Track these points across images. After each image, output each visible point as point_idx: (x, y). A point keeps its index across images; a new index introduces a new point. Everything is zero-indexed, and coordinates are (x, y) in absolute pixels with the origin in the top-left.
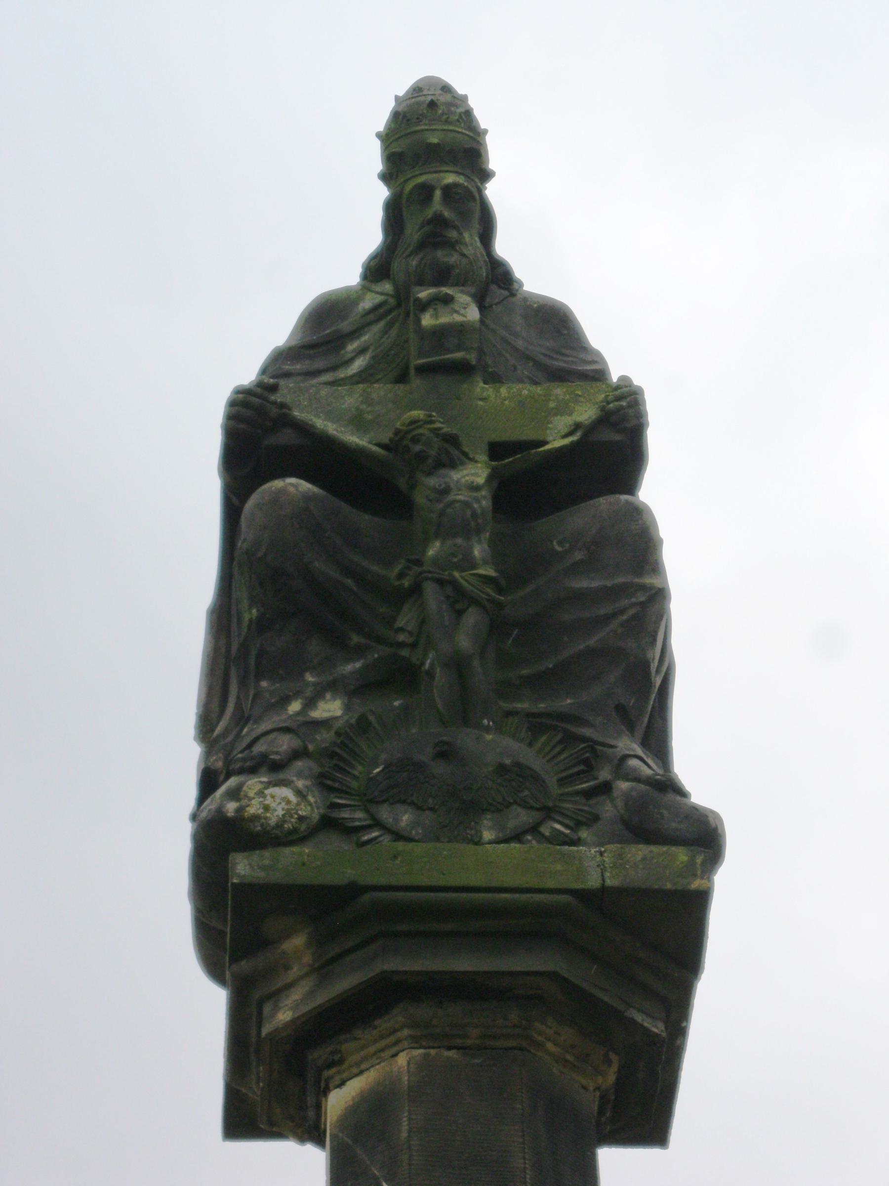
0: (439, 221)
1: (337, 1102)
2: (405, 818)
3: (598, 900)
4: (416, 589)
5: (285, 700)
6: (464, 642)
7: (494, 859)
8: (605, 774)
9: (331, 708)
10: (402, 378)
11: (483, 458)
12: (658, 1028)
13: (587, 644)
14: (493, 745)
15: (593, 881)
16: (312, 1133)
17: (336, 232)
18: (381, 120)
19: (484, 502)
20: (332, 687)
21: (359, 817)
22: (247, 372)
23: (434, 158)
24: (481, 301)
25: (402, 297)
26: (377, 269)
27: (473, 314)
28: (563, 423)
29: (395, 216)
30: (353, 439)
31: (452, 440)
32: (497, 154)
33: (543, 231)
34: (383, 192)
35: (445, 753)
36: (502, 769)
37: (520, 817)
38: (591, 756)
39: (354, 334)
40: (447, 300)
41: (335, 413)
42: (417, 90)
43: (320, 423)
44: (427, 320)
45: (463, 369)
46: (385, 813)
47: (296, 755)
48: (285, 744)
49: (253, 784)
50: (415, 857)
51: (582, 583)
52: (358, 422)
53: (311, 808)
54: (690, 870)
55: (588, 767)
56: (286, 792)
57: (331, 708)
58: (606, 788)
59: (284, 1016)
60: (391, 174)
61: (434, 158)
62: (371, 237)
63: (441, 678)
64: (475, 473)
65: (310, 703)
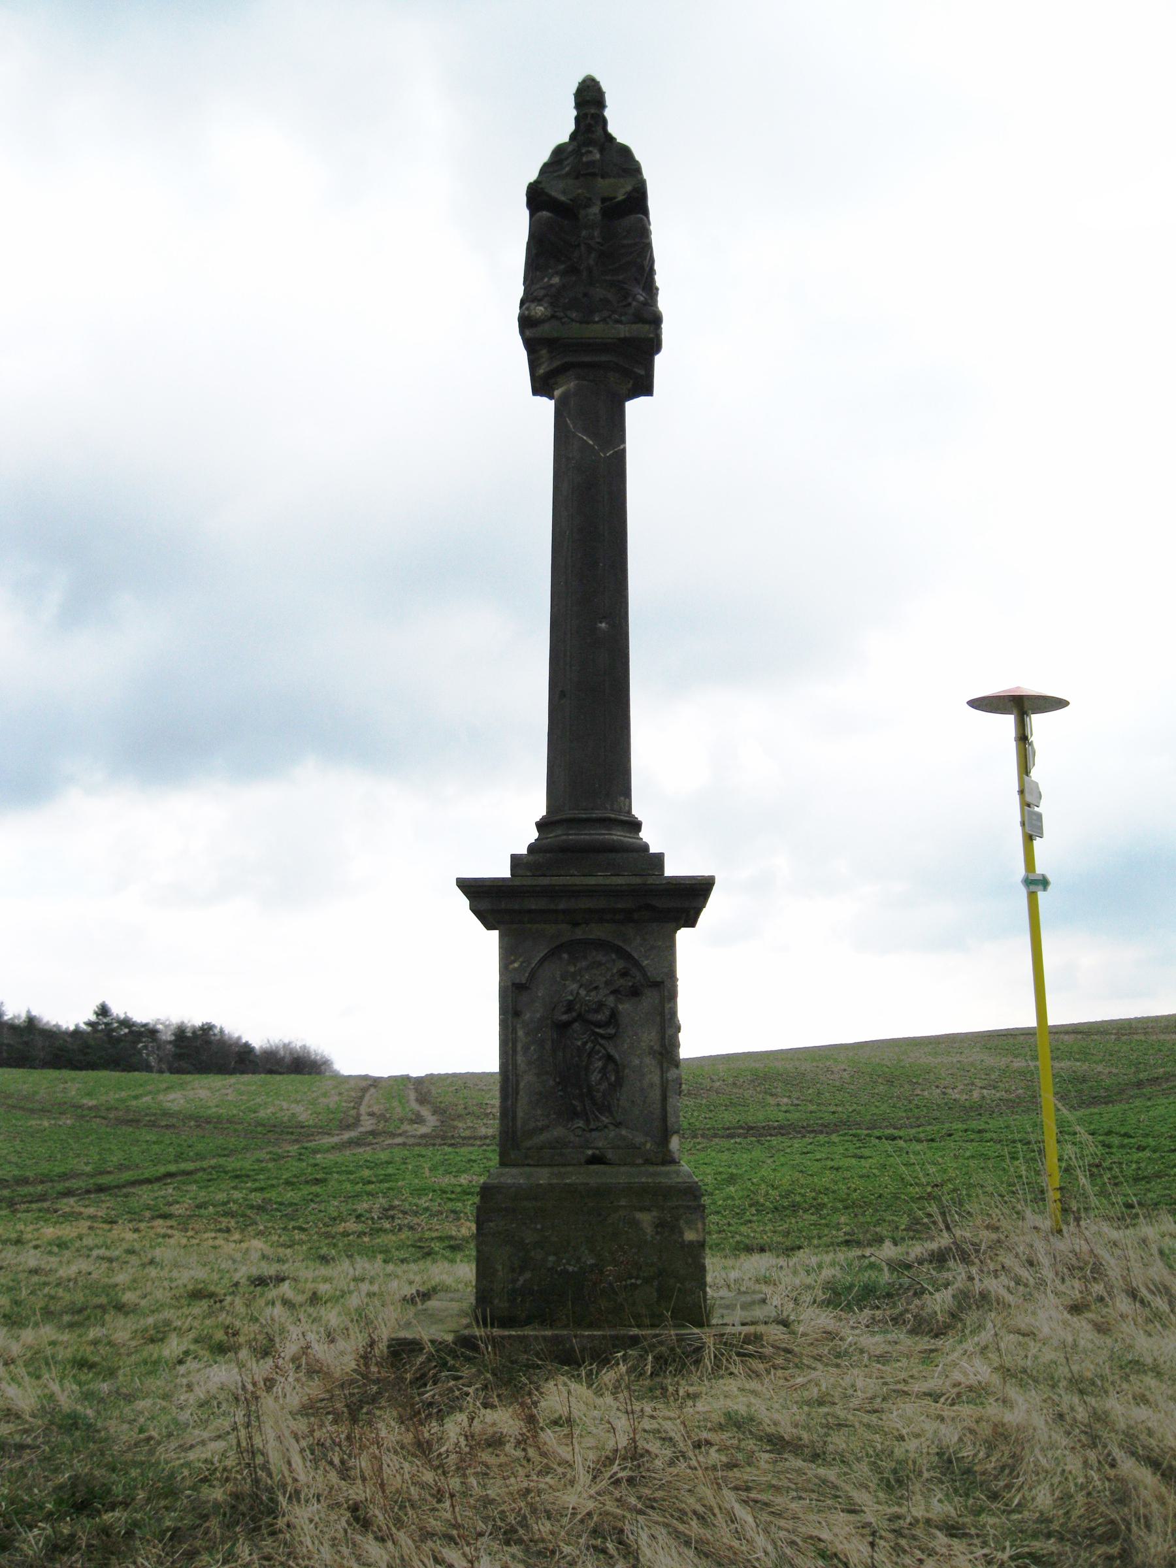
0: (590, 125)
1: (557, 393)
2: (574, 315)
3: (624, 341)
4: (579, 245)
5: (543, 279)
6: (591, 262)
7: (598, 330)
8: (630, 300)
9: (556, 280)
10: (577, 178)
11: (599, 203)
12: (642, 372)
13: (67, 1185)
14: (599, 293)
15: (622, 336)
16: (551, 397)
17: (561, 125)
18: (574, 90)
19: (599, 217)
20: (557, 273)
21: (562, 314)
22: (533, 175)
23: (590, 98)
24: (602, 151)
25: (579, 147)
26: (573, 136)
27: (598, 156)
28: (623, 191)
29: (578, 120)
30: (563, 198)
31: (590, 199)
32: (609, 100)
33: (621, 124)
34: (575, 113)
35: (585, 295)
36: (601, 300)
37: (605, 314)
38: (626, 295)
39: (567, 158)
40: (590, 152)
41: (557, 191)
42: (584, 81)
43: (553, 194)
44: (584, 159)
45: (594, 175)
46: (569, 313)
47: (545, 296)
48: (542, 292)
49: (533, 306)
50: (577, 331)
51: (625, 242)
52: (564, 193)
53: (548, 314)
54: (160, 1045)
55: (626, 298)
56: (541, 308)
57: (556, 280)
58: (630, 304)
59: (542, 371)
60: (578, 106)
61: (590, 98)
62: (571, 127)
63: (585, 274)
64: (595, 210)
65: (550, 279)
